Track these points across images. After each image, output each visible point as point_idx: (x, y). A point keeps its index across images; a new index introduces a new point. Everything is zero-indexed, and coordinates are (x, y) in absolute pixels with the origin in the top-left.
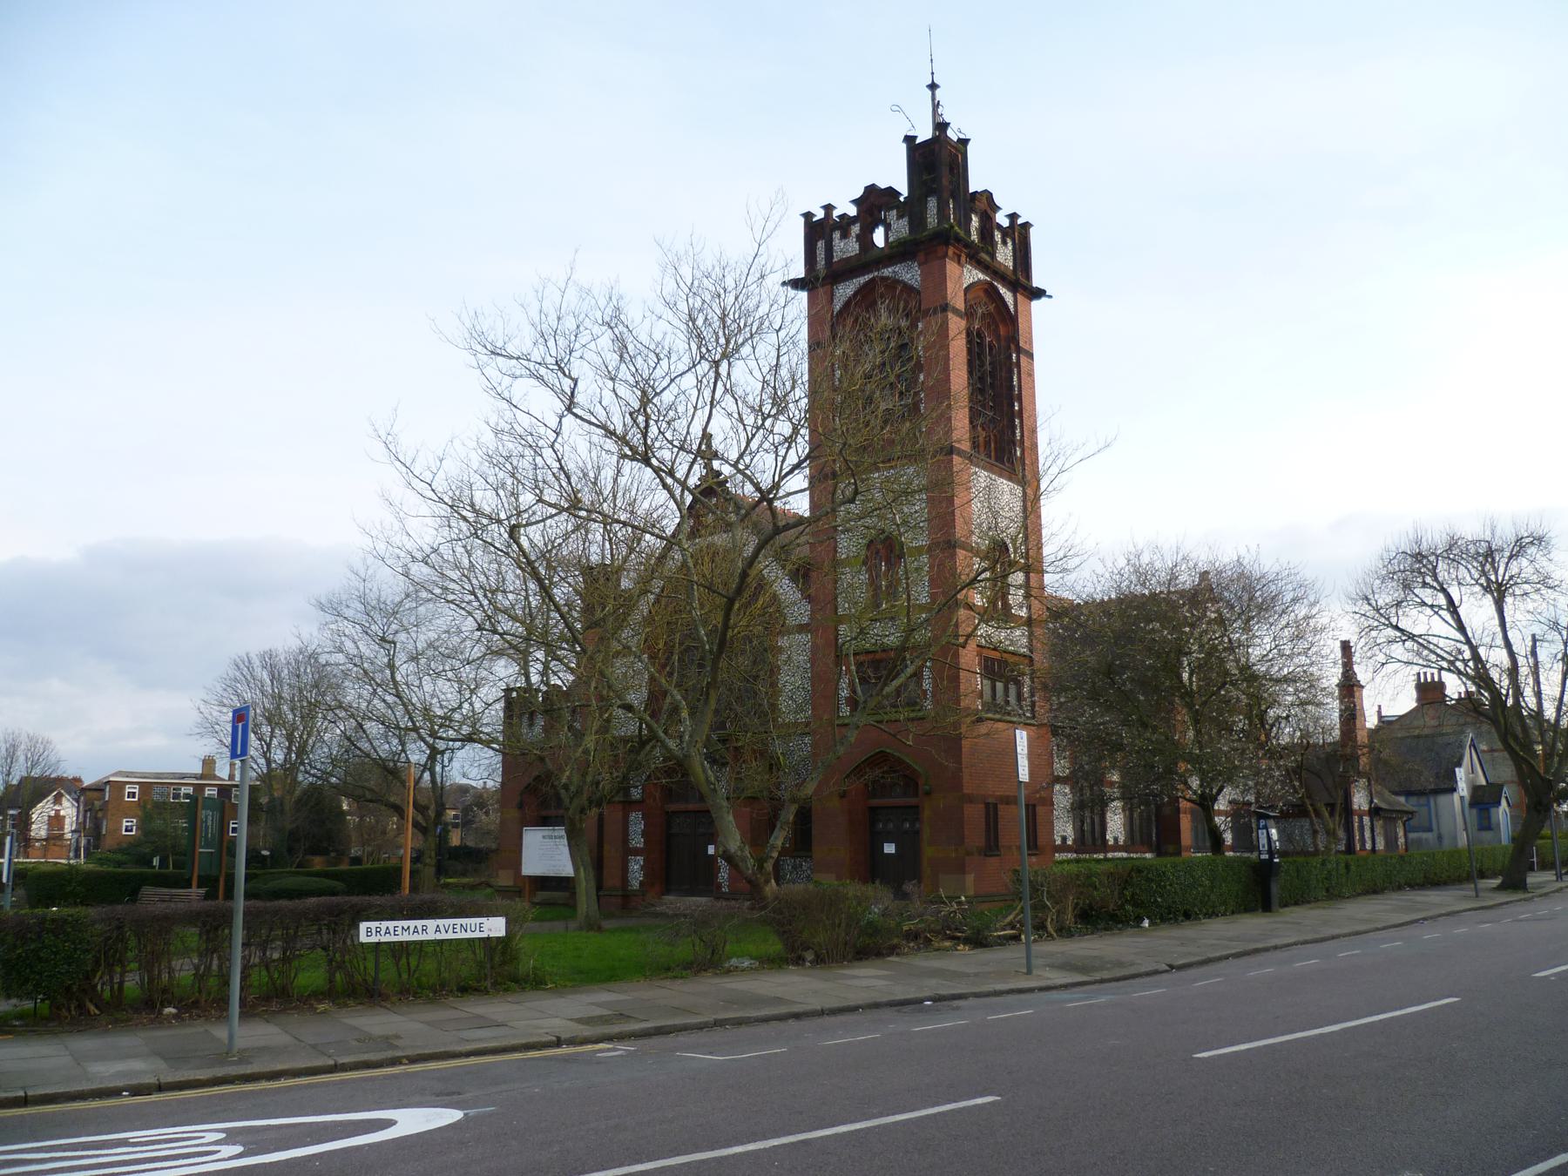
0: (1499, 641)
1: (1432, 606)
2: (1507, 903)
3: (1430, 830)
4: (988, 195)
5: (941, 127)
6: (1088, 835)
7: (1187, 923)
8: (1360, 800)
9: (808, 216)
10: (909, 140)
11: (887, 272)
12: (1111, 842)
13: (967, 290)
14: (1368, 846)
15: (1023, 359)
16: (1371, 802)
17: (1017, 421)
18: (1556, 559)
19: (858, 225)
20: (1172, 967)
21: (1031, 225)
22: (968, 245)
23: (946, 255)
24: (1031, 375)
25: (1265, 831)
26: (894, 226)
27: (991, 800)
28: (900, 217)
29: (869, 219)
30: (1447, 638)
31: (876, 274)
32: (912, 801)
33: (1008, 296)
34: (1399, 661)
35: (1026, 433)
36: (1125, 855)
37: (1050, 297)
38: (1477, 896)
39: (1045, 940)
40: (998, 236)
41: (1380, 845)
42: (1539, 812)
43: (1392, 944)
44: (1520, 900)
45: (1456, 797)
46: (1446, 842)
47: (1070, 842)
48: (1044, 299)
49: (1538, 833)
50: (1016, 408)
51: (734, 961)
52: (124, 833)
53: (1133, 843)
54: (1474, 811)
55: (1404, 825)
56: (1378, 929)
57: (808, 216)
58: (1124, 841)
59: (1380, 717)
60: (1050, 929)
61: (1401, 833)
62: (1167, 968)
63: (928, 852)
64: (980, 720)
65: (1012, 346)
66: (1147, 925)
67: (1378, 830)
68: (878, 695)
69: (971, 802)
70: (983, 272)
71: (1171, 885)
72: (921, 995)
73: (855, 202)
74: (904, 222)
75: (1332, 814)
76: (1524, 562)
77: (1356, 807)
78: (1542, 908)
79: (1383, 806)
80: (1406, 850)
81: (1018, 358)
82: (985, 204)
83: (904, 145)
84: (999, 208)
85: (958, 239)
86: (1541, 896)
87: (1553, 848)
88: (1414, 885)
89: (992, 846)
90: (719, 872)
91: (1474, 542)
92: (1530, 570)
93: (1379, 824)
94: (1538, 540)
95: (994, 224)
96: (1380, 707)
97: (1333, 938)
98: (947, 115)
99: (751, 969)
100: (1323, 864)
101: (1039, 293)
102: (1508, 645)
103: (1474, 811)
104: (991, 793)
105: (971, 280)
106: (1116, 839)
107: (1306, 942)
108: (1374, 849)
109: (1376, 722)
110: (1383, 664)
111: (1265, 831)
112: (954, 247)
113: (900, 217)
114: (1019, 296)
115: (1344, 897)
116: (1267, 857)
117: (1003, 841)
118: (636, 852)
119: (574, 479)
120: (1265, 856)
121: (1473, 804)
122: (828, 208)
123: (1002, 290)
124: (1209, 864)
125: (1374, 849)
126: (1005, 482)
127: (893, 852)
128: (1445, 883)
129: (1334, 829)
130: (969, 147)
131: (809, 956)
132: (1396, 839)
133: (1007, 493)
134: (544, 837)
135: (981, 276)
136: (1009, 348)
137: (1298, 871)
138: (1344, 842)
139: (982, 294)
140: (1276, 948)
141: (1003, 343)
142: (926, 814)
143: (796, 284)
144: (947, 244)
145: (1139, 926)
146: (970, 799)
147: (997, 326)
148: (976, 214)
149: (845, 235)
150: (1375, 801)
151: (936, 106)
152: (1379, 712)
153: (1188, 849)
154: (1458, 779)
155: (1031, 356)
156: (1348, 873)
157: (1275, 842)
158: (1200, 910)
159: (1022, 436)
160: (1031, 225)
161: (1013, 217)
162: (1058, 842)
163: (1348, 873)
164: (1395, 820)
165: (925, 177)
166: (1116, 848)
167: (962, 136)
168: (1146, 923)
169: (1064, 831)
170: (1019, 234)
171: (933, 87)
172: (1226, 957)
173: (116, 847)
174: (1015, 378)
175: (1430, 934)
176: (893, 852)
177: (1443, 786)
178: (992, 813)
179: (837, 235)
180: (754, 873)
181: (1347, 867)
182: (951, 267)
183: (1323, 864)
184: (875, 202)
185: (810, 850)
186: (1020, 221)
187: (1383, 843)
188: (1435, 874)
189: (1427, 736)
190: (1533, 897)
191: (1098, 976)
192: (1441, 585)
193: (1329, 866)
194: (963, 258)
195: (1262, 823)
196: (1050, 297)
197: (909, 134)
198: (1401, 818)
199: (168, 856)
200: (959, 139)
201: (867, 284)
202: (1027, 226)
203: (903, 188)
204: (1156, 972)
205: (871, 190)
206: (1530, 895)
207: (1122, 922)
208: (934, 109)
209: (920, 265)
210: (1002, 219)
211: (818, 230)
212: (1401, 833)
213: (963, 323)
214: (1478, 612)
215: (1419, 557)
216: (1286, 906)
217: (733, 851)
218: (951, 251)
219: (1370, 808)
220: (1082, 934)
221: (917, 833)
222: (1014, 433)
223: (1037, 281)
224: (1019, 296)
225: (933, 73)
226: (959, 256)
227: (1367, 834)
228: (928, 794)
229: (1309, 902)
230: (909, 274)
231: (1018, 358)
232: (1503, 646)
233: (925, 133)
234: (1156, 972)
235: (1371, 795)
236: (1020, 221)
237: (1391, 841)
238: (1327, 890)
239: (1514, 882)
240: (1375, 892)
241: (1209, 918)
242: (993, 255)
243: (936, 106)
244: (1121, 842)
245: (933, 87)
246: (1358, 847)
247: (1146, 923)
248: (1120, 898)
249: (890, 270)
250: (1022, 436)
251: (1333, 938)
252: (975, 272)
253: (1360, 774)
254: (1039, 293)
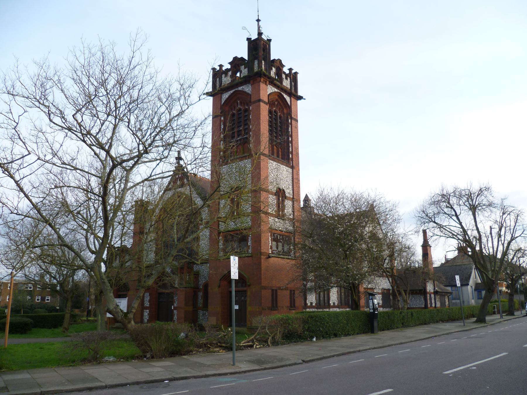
0: (475, 228)
1: (449, 215)
2: (475, 328)
3: (459, 299)
4: (280, 61)
5: (260, 34)
6: (322, 302)
7: (336, 338)
8: (430, 288)
9: (214, 69)
10: (249, 39)
11: (240, 88)
12: (332, 304)
13: (269, 95)
14: (433, 305)
15: (293, 122)
16: (435, 289)
17: (290, 144)
18: (494, 196)
19: (231, 72)
20: (303, 361)
21: (298, 73)
22: (270, 78)
23: (260, 81)
24: (297, 128)
25: (372, 300)
26: (243, 71)
27: (274, 288)
28: (245, 68)
29: (235, 70)
30: (455, 227)
31: (236, 89)
32: (245, 289)
33: (288, 98)
34: (437, 235)
35: (294, 149)
36: (316, 310)
37: (305, 99)
38: (464, 325)
39: (266, 347)
40: (284, 76)
41: (438, 305)
42: (490, 292)
43: (426, 345)
44: (482, 327)
45: (469, 287)
46: (466, 303)
47: (314, 305)
48: (302, 100)
49: (490, 301)
50: (290, 140)
51: (106, 358)
52: (46, 301)
53: (341, 305)
54: (476, 292)
55: (448, 297)
56: (412, 341)
57: (214, 69)
58: (338, 304)
59: (446, 259)
60: (269, 343)
61: (447, 300)
62: (302, 362)
63: (249, 308)
64: (269, 257)
65: (289, 117)
66: (315, 340)
67: (437, 299)
68: (182, 242)
69: (265, 289)
70: (277, 89)
71: (327, 323)
72: (164, 378)
73: (229, 63)
74: (246, 70)
75: (406, 294)
76: (483, 197)
77: (428, 291)
78: (490, 330)
79: (439, 290)
80: (449, 306)
81: (291, 121)
82: (278, 64)
83: (247, 42)
84: (284, 66)
85: (265, 75)
86: (491, 325)
87: (499, 305)
88: (443, 321)
89: (274, 306)
90: (174, 316)
91: (464, 190)
92: (485, 200)
93: (438, 298)
94: (487, 189)
95: (282, 72)
96: (446, 255)
97: (389, 346)
98: (262, 30)
99: (114, 362)
100: (401, 313)
101: (300, 98)
102: (477, 229)
103: (476, 292)
104: (275, 286)
105: (272, 91)
106: (334, 303)
107: (375, 348)
108: (435, 307)
109: (444, 261)
110: (432, 236)
111: (372, 300)
112: (264, 78)
113: (245, 68)
114: (292, 98)
115: (410, 326)
116: (372, 311)
117: (279, 304)
118: (146, 308)
119: (28, 143)
120: (372, 311)
121: (475, 290)
122: (221, 66)
123: (285, 96)
124: (346, 314)
125: (435, 307)
126: (284, 167)
127: (238, 308)
128: (458, 320)
129: (407, 300)
130: (271, 43)
131: (148, 355)
132: (445, 303)
133: (285, 171)
135: (276, 90)
136: (288, 117)
137: (389, 316)
138: (424, 304)
139: (277, 97)
140: (359, 351)
141: (285, 116)
142: (249, 293)
143: (208, 94)
144: (261, 77)
145: (311, 341)
146: (265, 288)
147: (283, 109)
148: (274, 67)
149: (226, 76)
150: (436, 289)
151: (259, 27)
152: (445, 257)
153: (363, 307)
154: (456, 280)
155: (297, 121)
156: (412, 317)
157: (376, 305)
158: (342, 333)
159: (292, 150)
160: (298, 73)
161: (290, 70)
162: (309, 304)
163: (412, 317)
164: (444, 295)
165: (254, 53)
166: (334, 306)
167: (268, 38)
168: (314, 339)
169: (311, 300)
170: (293, 77)
171: (258, 20)
172: (333, 356)
173: (4, 306)
174: (290, 129)
175: (441, 343)
176: (238, 308)
177: (464, 283)
178: (274, 293)
179: (223, 76)
180: (122, 319)
181: (412, 314)
182: (262, 86)
183: (401, 313)
184: (237, 63)
185: (208, 308)
186: (293, 72)
187: (439, 304)
188: (453, 316)
189: (459, 265)
190: (488, 325)
191: (264, 366)
192: (451, 206)
193: (403, 314)
194: (268, 82)
195: (371, 297)
196: (305, 99)
197: (249, 37)
198: (447, 295)
199: (21, 309)
200: (267, 39)
201: (232, 94)
202: (296, 73)
203: (246, 57)
204: (295, 364)
205: (235, 59)
206: (486, 325)
207: (304, 339)
208: (258, 29)
209: (251, 85)
210: (286, 70)
211: (217, 74)
212: (447, 300)
213: (267, 107)
214: (467, 218)
215: (443, 196)
216: (383, 330)
217: (111, 309)
218: (262, 80)
219: (434, 291)
220: (283, 344)
221: (246, 301)
222: (289, 149)
224: (292, 98)
225: (258, 16)
226: (266, 82)
227: (433, 301)
228: (249, 286)
229: (394, 329)
230: (247, 89)
231: (291, 121)
232: (476, 229)
233: (254, 36)
234: (295, 364)
235: (434, 285)
236: (293, 72)
237: (443, 304)
238: (403, 324)
239: (481, 320)
240: (425, 324)
241: (346, 336)
242: (281, 83)
243: (259, 27)
244: (336, 304)
245: (258, 20)
246: (429, 306)
247: (314, 339)
248: (303, 329)
249: (241, 87)
250: (292, 150)
251: (389, 346)
252: (273, 88)
253: (430, 279)
254: (300, 98)
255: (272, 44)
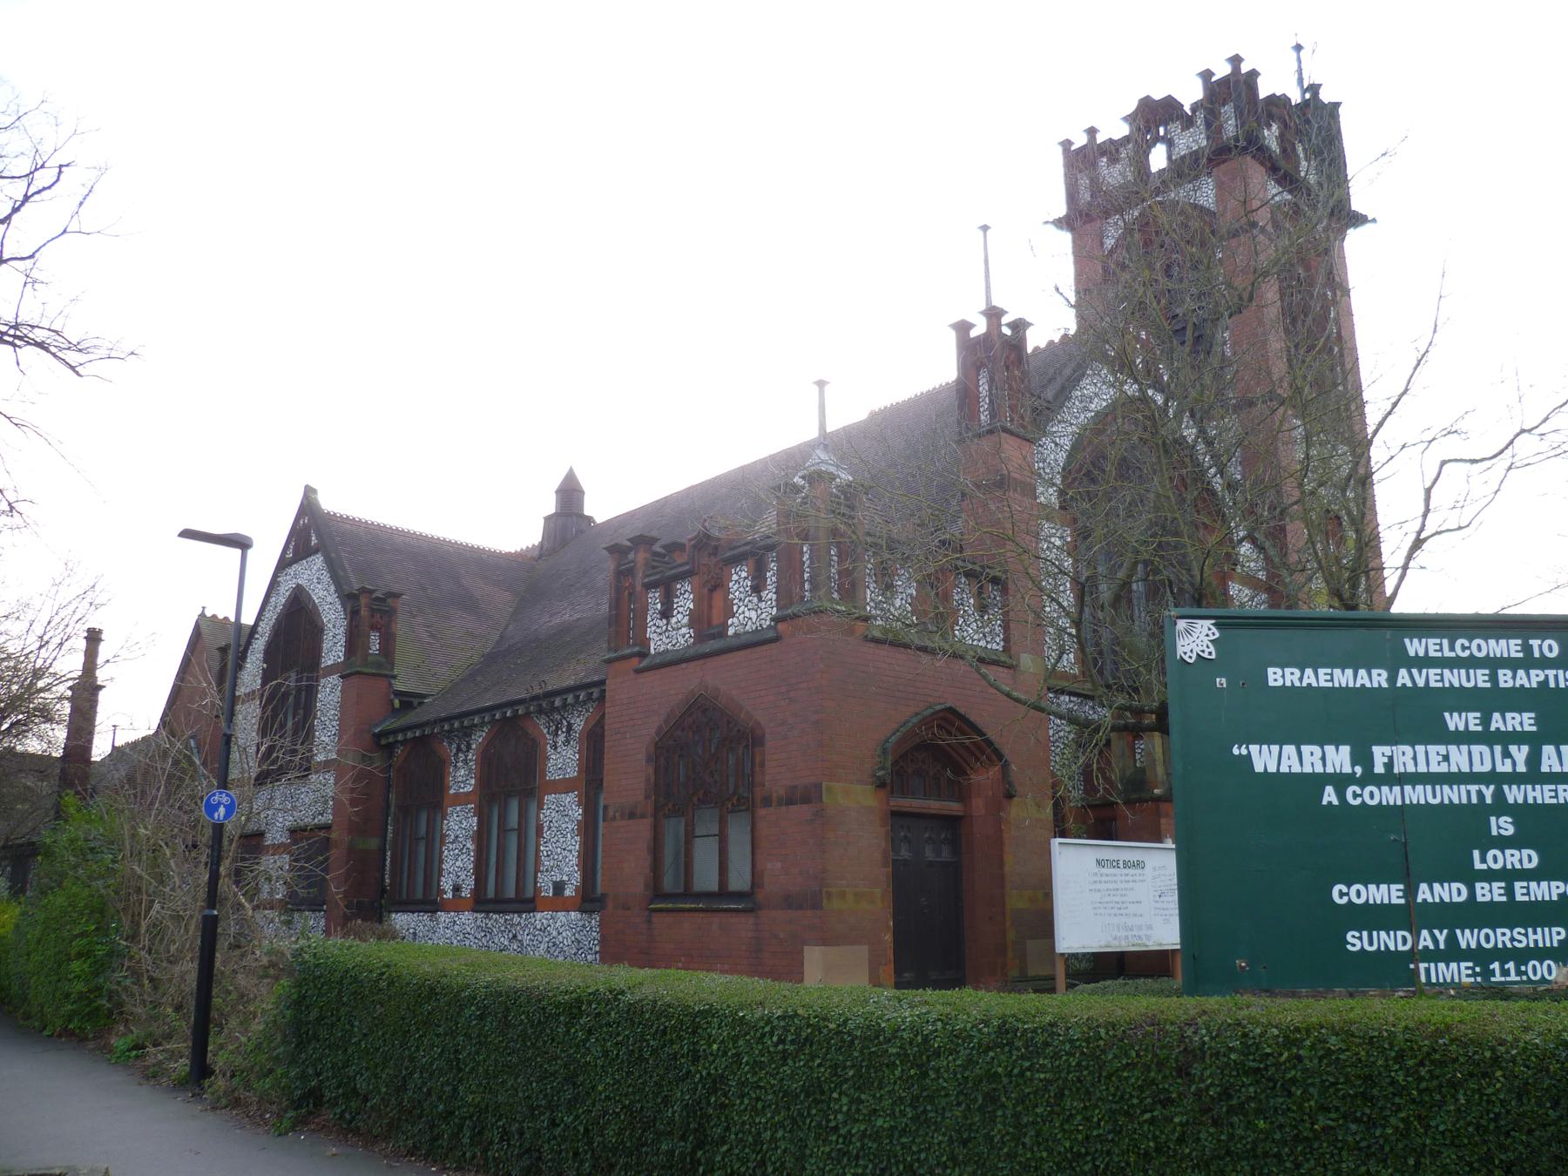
101: (1358, 220)
134: (1098, 862)
196: (1374, 220)
205: (1147, 105)
223: (1357, 205)
254: (1358, 220)
255: (1341, 110)
